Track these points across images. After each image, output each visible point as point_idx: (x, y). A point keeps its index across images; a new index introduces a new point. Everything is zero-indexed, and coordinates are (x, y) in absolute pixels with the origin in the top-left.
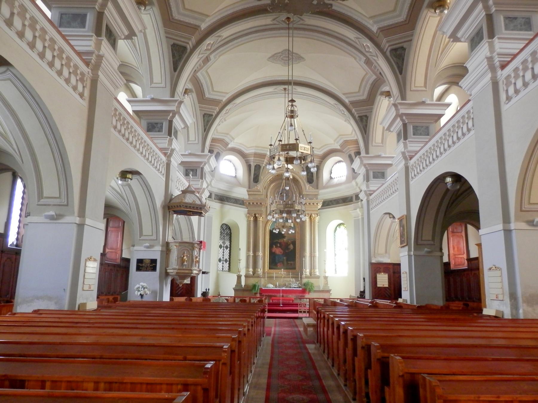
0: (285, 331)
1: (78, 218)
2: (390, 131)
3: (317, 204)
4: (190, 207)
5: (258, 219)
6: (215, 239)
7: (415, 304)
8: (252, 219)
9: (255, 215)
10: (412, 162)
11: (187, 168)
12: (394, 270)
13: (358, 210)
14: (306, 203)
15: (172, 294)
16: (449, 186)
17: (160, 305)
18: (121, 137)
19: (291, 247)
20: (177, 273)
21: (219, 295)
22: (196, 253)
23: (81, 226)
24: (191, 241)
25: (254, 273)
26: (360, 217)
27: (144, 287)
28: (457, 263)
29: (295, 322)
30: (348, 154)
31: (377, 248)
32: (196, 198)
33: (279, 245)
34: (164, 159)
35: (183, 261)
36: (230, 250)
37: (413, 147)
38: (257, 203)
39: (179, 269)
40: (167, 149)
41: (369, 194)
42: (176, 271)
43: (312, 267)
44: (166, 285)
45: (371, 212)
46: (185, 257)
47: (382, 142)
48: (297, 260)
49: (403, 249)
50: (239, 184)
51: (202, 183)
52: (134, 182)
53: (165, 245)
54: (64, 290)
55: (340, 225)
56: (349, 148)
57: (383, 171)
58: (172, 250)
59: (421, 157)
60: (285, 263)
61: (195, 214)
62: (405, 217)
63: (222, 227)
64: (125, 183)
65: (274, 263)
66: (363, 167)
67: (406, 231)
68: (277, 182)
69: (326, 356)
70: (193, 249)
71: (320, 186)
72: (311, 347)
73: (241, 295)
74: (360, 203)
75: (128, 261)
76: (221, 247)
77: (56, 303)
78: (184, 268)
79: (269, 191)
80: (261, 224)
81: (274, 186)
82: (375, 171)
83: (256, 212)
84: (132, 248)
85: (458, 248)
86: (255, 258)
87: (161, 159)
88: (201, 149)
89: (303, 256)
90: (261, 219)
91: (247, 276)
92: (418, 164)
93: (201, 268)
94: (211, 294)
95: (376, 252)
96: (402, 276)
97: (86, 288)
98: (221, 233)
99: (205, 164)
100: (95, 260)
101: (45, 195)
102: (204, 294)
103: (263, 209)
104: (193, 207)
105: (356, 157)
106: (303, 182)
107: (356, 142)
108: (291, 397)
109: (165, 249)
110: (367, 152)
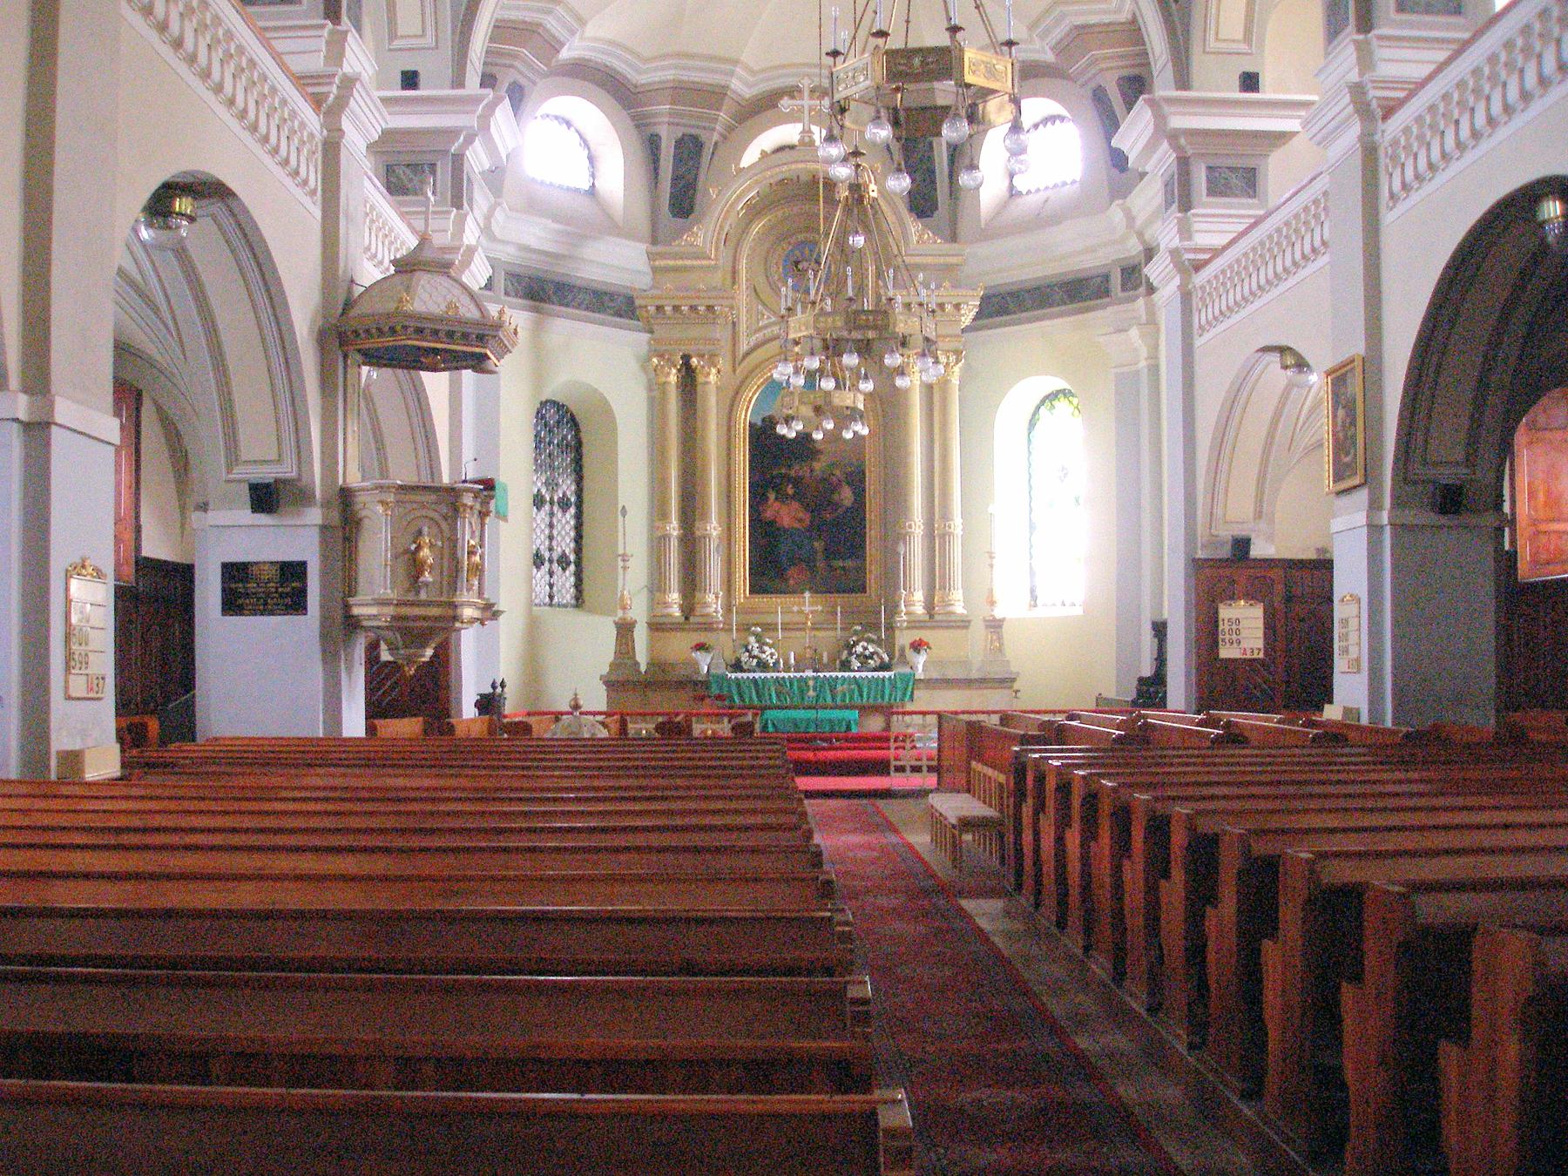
0: (851, 848)
1: (23, 399)
3: (957, 307)
4: (436, 332)
5: (700, 379)
6: (517, 471)
7: (1389, 724)
8: (673, 378)
9: (686, 358)
11: (392, 160)
13: (1134, 333)
14: (941, 306)
15: (375, 711)
16: (1553, 234)
17: (325, 753)
18: (153, 36)
19: (846, 496)
20: (394, 618)
21: (576, 707)
22: (467, 537)
24: (425, 480)
25: (688, 609)
26: (1143, 364)
27: (266, 683)
28: (1544, 556)
29: (879, 812)
30: (1093, 85)
32: (457, 291)
33: (790, 491)
34: (312, 120)
35: (415, 568)
36: (579, 516)
42: (390, 610)
43: (936, 582)
44: (350, 671)
45: (1199, 342)
46: (425, 552)
47: (1247, 37)
48: (872, 550)
49: (1345, 500)
50: (612, 227)
51: (460, 224)
52: (197, 230)
53: (336, 503)
55: (1053, 396)
57: (1249, 163)
58: (366, 522)
59: (1432, 109)
60: (821, 564)
61: (454, 361)
62: (1358, 364)
63: (540, 415)
65: (770, 569)
66: (1165, 145)
67: (1360, 423)
69: (1073, 942)
70: (455, 510)
71: (964, 228)
72: (985, 912)
73: (666, 707)
74: (1141, 302)
75: (181, 576)
76: (538, 501)
78: (423, 596)
80: (712, 400)
81: (771, 228)
84: (195, 517)
85: (1549, 493)
86: (691, 545)
87: (303, 125)
89: (895, 536)
90: (712, 378)
91: (656, 627)
92: (1421, 137)
94: (511, 707)
95: (1219, 512)
96: (1339, 611)
97: (78, 686)
98: (538, 441)
99: (469, 141)
100: (99, 574)
102: (488, 704)
103: (721, 333)
104: (450, 334)
105: (1129, 105)
106: (896, 213)
107: (1133, 31)
108: (966, 1097)
109: (335, 517)
110: (1183, 82)
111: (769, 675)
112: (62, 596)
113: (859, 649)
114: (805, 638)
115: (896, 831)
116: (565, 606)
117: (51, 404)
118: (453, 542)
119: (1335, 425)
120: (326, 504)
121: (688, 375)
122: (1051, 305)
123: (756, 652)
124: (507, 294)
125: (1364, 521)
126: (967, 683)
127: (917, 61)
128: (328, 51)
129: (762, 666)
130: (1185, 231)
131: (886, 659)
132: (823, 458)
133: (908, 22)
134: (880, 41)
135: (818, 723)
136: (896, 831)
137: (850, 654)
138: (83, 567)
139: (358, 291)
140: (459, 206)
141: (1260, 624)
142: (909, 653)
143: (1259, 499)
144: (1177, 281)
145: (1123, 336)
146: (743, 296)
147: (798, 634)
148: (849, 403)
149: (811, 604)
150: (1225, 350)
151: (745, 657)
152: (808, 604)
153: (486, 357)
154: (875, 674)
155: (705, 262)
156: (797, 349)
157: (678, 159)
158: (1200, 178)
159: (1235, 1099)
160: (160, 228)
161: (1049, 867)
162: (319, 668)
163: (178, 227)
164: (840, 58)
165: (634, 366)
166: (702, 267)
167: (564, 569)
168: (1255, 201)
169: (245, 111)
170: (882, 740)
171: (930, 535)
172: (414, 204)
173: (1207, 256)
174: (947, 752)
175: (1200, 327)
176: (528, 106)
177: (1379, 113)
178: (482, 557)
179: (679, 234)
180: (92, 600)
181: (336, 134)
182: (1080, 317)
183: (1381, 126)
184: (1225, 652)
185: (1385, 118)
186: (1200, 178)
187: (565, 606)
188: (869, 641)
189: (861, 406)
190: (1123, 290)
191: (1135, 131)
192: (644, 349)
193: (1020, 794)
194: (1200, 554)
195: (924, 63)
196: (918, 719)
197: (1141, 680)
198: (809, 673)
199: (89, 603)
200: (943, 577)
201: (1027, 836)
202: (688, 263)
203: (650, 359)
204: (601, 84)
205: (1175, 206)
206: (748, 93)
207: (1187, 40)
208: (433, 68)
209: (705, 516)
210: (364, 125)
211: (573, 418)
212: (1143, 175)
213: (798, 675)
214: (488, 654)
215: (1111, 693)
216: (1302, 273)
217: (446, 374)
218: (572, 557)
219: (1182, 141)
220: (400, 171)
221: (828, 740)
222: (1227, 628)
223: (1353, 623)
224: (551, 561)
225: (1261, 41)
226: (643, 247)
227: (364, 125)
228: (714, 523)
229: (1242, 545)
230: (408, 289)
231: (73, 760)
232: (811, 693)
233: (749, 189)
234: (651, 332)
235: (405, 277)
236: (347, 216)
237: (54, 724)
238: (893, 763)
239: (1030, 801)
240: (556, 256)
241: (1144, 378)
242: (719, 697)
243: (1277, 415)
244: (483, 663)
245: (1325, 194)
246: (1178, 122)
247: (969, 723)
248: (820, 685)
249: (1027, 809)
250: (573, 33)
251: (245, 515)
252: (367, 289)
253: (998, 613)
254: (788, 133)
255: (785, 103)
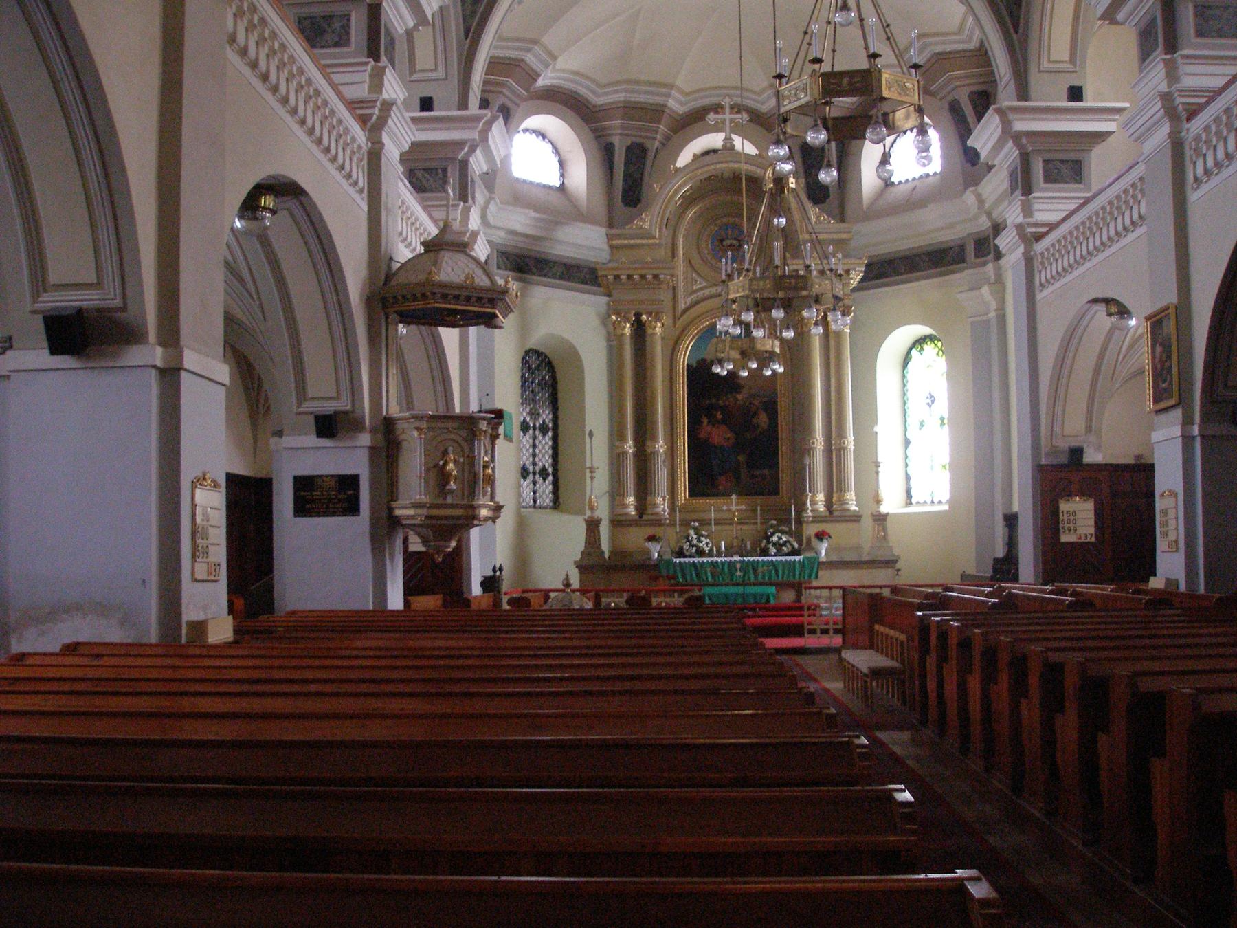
1: (159, 351)
2: (1114, 22)
3: (848, 272)
5: (649, 331)
9: (638, 315)
10: (1196, 126)
12: (1126, 489)
13: (985, 290)
17: (377, 621)
18: (247, 71)
19: (763, 419)
20: (426, 517)
23: (170, 375)
24: (442, 411)
25: (642, 508)
26: (992, 314)
27: (327, 568)
30: (950, 98)
31: (1059, 418)
32: (472, 265)
33: (719, 416)
35: (443, 477)
36: (555, 439)
37: (1199, 76)
38: (643, 277)
39: (432, 506)
40: (370, 103)
41: (1030, 237)
42: (424, 512)
43: (835, 485)
45: (1040, 296)
46: (451, 466)
47: (1072, 60)
48: (784, 462)
49: (1163, 417)
50: (575, 214)
52: (276, 220)
54: (144, 581)
55: (920, 342)
56: (952, 79)
57: (1072, 156)
58: (405, 445)
60: (743, 472)
62: (1172, 311)
63: (525, 362)
64: (253, 225)
65: (705, 479)
66: (1010, 144)
68: (707, 202)
71: (850, 210)
74: (990, 266)
77: (122, 623)
78: (449, 500)
79: (682, 232)
80: (658, 349)
81: (699, 216)
82: (1048, 156)
83: (640, 308)
86: (643, 460)
87: (354, 140)
88: (455, 97)
89: (802, 450)
90: (658, 330)
92: (1218, 134)
93: (497, 499)
95: (1057, 428)
96: (1159, 504)
97: (201, 572)
98: (524, 381)
99: (473, 150)
101: (53, 278)
102: (490, 584)
103: (665, 296)
104: (468, 298)
105: (980, 116)
107: (981, 56)
111: (705, 560)
112: (189, 500)
113: (775, 539)
114: (734, 531)
115: (816, 680)
116: (545, 508)
117: (181, 357)
118: (471, 459)
119: (1154, 358)
120: (373, 431)
121: (640, 330)
122: (918, 271)
123: (695, 542)
124: (499, 268)
125: (1179, 434)
126: (858, 564)
127: (845, 81)
128: (371, 82)
129: (700, 553)
130: (1027, 210)
131: (796, 545)
132: (745, 391)
133: (834, 51)
134: (817, 66)
135: (744, 596)
136: (816, 680)
137: (768, 542)
138: (204, 479)
139: (396, 266)
140: (465, 201)
141: (1091, 515)
142: (814, 541)
143: (1089, 418)
144: (1021, 249)
145: (976, 293)
146: (680, 266)
147: (727, 527)
148: (768, 348)
149: (737, 504)
150: (1061, 302)
151: (686, 546)
152: (734, 505)
153: (495, 316)
154: (788, 558)
155: (651, 241)
156: (734, 306)
157: (627, 163)
158: (1038, 168)
159: (1128, 884)
160: (249, 219)
161: (952, 709)
162: (369, 557)
163: (264, 218)
164: (784, 80)
165: (595, 322)
166: (648, 245)
167: (544, 480)
168: (1081, 186)
169: (313, 128)
170: (797, 608)
171: (828, 451)
172: (438, 199)
173: (1044, 230)
174: (849, 619)
175: (1041, 285)
176: (514, 121)
177: (1184, 115)
178: (493, 469)
179: (630, 220)
180: (211, 505)
181: (377, 146)
182: (941, 279)
183: (1186, 126)
184: (1065, 538)
185: (1189, 119)
186: (1038, 168)
187: (545, 508)
188: (783, 532)
189: (777, 350)
190: (976, 256)
191: (985, 136)
192: (603, 309)
193: (924, 650)
194: (1043, 462)
195: (850, 84)
196: (825, 593)
197: (996, 560)
198: (737, 558)
199: (209, 506)
200: (839, 482)
201: (931, 685)
202: (639, 241)
203: (609, 316)
204: (566, 105)
205: (1018, 192)
206: (681, 110)
207: (1025, 60)
208: (445, 95)
209: (654, 438)
210: (399, 137)
211: (550, 363)
212: (990, 168)
213: (728, 559)
214: (488, 547)
215: (972, 571)
216: (1124, 241)
217: (457, 330)
218: (550, 470)
219: (1024, 141)
220: (419, 174)
221: (753, 609)
222: (1065, 518)
223: (1172, 513)
224: (534, 473)
225: (1084, 62)
226: (603, 230)
227: (399, 137)
228: (631, 443)
229: (1077, 453)
230: (435, 263)
231: (199, 628)
232: (738, 573)
233: (685, 184)
234: (609, 295)
235: (432, 255)
236: (386, 208)
237: (184, 601)
238: (807, 627)
239: (934, 655)
240: (533, 237)
241: (994, 322)
242: (669, 578)
243: (1101, 356)
244: (486, 551)
245: (1141, 179)
246: (1020, 126)
247: (871, 595)
248: (745, 567)
249: (931, 662)
250: (547, 66)
251: (312, 440)
252: (404, 265)
253: (884, 509)
254: (714, 140)
255: (711, 118)
